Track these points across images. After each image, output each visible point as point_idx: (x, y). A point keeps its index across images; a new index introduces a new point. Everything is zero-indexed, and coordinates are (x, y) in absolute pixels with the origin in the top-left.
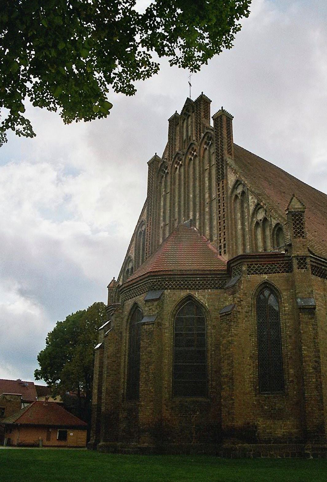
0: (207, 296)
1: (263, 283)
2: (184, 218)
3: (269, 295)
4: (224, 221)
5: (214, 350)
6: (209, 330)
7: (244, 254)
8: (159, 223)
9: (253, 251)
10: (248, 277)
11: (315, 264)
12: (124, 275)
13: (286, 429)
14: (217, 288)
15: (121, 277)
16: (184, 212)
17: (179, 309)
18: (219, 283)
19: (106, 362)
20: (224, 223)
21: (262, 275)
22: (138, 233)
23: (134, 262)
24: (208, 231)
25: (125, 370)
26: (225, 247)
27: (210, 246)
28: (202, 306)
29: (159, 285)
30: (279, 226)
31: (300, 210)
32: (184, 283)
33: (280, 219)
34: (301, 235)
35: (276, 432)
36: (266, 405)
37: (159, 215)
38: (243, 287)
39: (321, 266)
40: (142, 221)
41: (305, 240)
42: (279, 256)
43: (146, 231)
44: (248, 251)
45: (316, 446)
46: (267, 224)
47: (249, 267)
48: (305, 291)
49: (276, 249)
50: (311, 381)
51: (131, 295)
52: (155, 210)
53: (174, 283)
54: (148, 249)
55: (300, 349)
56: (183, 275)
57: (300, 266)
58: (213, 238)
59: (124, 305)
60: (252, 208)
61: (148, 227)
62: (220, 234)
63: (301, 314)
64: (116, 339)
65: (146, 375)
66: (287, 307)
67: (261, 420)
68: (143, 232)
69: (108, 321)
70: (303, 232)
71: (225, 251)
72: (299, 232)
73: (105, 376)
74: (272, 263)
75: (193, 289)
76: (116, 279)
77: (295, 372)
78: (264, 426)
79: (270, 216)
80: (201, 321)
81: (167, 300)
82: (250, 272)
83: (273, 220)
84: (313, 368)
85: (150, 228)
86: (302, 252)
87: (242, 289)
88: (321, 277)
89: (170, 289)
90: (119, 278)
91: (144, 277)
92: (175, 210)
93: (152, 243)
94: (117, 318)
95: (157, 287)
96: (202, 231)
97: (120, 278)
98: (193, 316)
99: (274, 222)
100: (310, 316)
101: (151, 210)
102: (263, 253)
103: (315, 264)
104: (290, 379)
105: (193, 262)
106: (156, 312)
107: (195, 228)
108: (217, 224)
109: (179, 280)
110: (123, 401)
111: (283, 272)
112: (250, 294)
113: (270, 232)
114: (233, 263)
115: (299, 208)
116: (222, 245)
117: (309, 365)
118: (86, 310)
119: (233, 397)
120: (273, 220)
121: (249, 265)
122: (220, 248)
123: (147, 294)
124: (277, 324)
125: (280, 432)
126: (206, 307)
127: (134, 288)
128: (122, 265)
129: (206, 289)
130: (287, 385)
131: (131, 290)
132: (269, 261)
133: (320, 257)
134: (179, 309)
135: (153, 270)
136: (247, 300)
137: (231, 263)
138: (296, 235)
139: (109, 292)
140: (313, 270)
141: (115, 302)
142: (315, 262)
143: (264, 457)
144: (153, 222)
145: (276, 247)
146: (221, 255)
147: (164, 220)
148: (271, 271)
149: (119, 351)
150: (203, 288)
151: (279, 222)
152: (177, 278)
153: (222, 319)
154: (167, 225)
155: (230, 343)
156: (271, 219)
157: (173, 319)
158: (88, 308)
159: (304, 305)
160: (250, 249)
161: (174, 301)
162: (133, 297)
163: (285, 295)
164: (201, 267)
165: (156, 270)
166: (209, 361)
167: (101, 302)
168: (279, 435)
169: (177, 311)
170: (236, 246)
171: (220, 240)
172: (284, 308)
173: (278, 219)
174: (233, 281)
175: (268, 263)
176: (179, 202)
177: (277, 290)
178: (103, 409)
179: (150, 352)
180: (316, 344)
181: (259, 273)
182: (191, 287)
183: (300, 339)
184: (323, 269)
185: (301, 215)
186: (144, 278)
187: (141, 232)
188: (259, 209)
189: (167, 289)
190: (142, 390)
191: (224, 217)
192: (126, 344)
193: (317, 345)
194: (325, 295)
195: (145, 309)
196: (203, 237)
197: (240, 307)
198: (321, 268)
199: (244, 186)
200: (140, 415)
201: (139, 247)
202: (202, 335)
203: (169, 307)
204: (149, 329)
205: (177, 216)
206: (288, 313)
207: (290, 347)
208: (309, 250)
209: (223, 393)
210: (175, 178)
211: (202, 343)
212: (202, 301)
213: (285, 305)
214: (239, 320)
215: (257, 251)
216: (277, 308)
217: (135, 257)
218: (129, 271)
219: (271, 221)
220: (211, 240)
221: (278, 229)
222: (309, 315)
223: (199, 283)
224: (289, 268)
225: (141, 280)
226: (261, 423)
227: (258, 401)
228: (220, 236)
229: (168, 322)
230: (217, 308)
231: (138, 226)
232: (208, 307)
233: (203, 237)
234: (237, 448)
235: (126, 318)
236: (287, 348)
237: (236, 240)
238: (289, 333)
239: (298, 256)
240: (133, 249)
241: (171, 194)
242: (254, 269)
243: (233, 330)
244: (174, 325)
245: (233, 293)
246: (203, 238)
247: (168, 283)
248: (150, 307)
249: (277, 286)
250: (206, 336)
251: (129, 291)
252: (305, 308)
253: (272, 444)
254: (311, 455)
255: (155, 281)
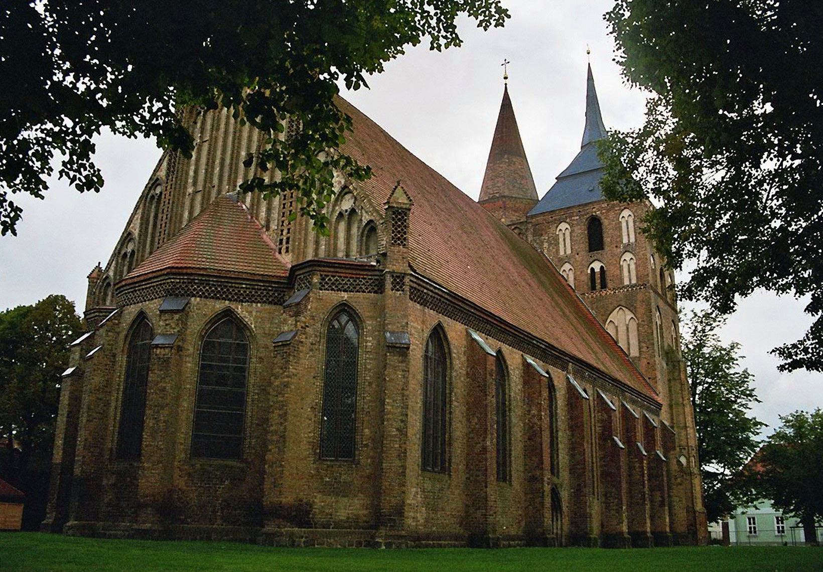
0: (254, 313)
1: (341, 304)
2: (227, 187)
3: (347, 322)
4: (291, 203)
5: (258, 394)
6: (254, 364)
7: (316, 259)
8: (185, 188)
9: (329, 256)
10: (319, 293)
11: (415, 285)
12: (117, 261)
13: (352, 510)
14: (270, 303)
15: (112, 262)
16: (230, 176)
17: (210, 328)
18: (273, 296)
19: (86, 399)
20: (291, 206)
21: (339, 292)
22: (149, 196)
23: (137, 243)
24: (264, 214)
25: (116, 414)
26: (287, 242)
27: (265, 237)
28: (246, 327)
29: (183, 289)
30: (372, 224)
31: (404, 206)
32: (222, 289)
33: (374, 214)
34: (402, 242)
35: (338, 514)
36: (328, 475)
37: (187, 174)
38: (311, 308)
39: (422, 289)
40: (158, 179)
41: (405, 250)
42: (367, 268)
43: (163, 196)
44: (322, 254)
45: (392, 533)
46: (356, 219)
47: (323, 279)
48: (398, 322)
49: (364, 258)
50: (392, 448)
51: (135, 298)
52: (181, 166)
53: (207, 288)
54: (164, 225)
55: (383, 403)
56: (222, 277)
57: (395, 286)
58: (271, 226)
59: (122, 312)
60: (336, 189)
61: (166, 190)
62: (283, 222)
63: (388, 354)
64: (106, 365)
65: (154, 424)
66: (370, 342)
67: (319, 496)
68: (156, 197)
69: (87, 332)
70: (405, 239)
71: (287, 248)
72: (400, 237)
73: (84, 421)
74: (357, 278)
75: (234, 301)
76: (103, 266)
77: (371, 433)
78: (323, 504)
79: (360, 207)
80: (243, 349)
81: (194, 314)
82: (324, 286)
83: (364, 214)
84: (398, 430)
85: (170, 192)
86: (400, 267)
87: (309, 310)
88: (421, 305)
89: (200, 296)
90: (109, 264)
91: (160, 273)
92: (213, 172)
93: (171, 217)
94: (109, 331)
95: (180, 292)
96: (255, 212)
97: (110, 266)
98: (230, 341)
99: (366, 218)
100: (401, 358)
101: (174, 164)
102: (345, 260)
103: (415, 285)
104: (365, 443)
105: (238, 260)
106: (176, 330)
107: (244, 206)
108: (280, 205)
109: (215, 285)
110: (110, 460)
111: (369, 292)
112: (321, 318)
113: (358, 230)
114: (300, 269)
115: (404, 204)
116: (285, 238)
117: (392, 425)
118: (34, 306)
119: (283, 463)
120: (364, 214)
121: (323, 276)
122: (281, 243)
123: (164, 301)
124: (354, 364)
125: (342, 515)
126: (252, 329)
127: (141, 288)
128: (116, 245)
129: (255, 302)
130: (360, 450)
131: (136, 291)
132: (352, 274)
133: (423, 276)
134: (210, 328)
135: (177, 265)
136: (315, 327)
137: (297, 270)
138: (395, 242)
139: (89, 285)
140: (411, 293)
141: (98, 302)
142: (415, 283)
143: (319, 546)
144: (176, 184)
145: (364, 253)
146: (280, 253)
147: (195, 184)
148: (353, 288)
149: (108, 383)
150: (250, 300)
151: (373, 218)
152: (213, 281)
153: (277, 351)
154: (199, 191)
155: (286, 385)
156: (361, 212)
157: (200, 343)
158: (37, 302)
159: (394, 341)
160: (325, 251)
161: (205, 315)
162: (138, 303)
163: (369, 325)
164: (249, 268)
165: (182, 265)
166: (250, 408)
167: (62, 296)
168: (341, 518)
169: (207, 330)
170: (305, 243)
171: (282, 231)
172: (366, 343)
173: (372, 214)
174: (296, 297)
175: (350, 275)
176: (223, 160)
177: (359, 317)
178: (77, 471)
179: (163, 390)
180: (405, 398)
181: (336, 289)
182: (233, 297)
183: (384, 389)
184: (425, 293)
185: (405, 214)
186: (161, 276)
187: (153, 197)
188: (346, 194)
189: (196, 296)
190: (147, 446)
191: (292, 197)
192: (120, 373)
193: (406, 399)
194: (423, 330)
195: (159, 324)
196: (256, 221)
197: (304, 336)
198: (423, 291)
199: (327, 154)
200: (142, 482)
201: (148, 220)
202: (242, 369)
203: (196, 325)
204: (164, 355)
205: (216, 181)
206: (370, 350)
207: (369, 398)
208: (410, 266)
209: (269, 457)
210: (219, 119)
211: (241, 382)
212: (246, 320)
213: (368, 339)
214: (301, 354)
215: (335, 255)
216: (355, 341)
217: (140, 235)
218: (127, 255)
219: (362, 216)
220: (268, 228)
221: (371, 229)
222: (399, 357)
223: (245, 292)
224: (379, 288)
225: (155, 277)
226: (319, 501)
227: (317, 469)
228: (282, 225)
229: (192, 347)
230: (266, 332)
231: (150, 185)
232: (254, 330)
233: (256, 221)
234: (283, 533)
235: (125, 333)
236: (365, 399)
237: (306, 234)
238: (369, 378)
239: (394, 272)
240: (137, 222)
241: (210, 145)
242: (330, 283)
243: (291, 367)
244: (201, 352)
245: (297, 314)
246: (255, 222)
247: (198, 287)
248: (167, 322)
249: (360, 311)
250: (247, 372)
251: (132, 292)
252: (395, 347)
253: (331, 530)
254: (383, 544)
255: (177, 282)
